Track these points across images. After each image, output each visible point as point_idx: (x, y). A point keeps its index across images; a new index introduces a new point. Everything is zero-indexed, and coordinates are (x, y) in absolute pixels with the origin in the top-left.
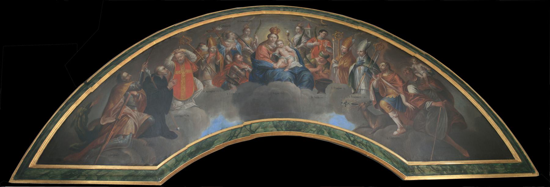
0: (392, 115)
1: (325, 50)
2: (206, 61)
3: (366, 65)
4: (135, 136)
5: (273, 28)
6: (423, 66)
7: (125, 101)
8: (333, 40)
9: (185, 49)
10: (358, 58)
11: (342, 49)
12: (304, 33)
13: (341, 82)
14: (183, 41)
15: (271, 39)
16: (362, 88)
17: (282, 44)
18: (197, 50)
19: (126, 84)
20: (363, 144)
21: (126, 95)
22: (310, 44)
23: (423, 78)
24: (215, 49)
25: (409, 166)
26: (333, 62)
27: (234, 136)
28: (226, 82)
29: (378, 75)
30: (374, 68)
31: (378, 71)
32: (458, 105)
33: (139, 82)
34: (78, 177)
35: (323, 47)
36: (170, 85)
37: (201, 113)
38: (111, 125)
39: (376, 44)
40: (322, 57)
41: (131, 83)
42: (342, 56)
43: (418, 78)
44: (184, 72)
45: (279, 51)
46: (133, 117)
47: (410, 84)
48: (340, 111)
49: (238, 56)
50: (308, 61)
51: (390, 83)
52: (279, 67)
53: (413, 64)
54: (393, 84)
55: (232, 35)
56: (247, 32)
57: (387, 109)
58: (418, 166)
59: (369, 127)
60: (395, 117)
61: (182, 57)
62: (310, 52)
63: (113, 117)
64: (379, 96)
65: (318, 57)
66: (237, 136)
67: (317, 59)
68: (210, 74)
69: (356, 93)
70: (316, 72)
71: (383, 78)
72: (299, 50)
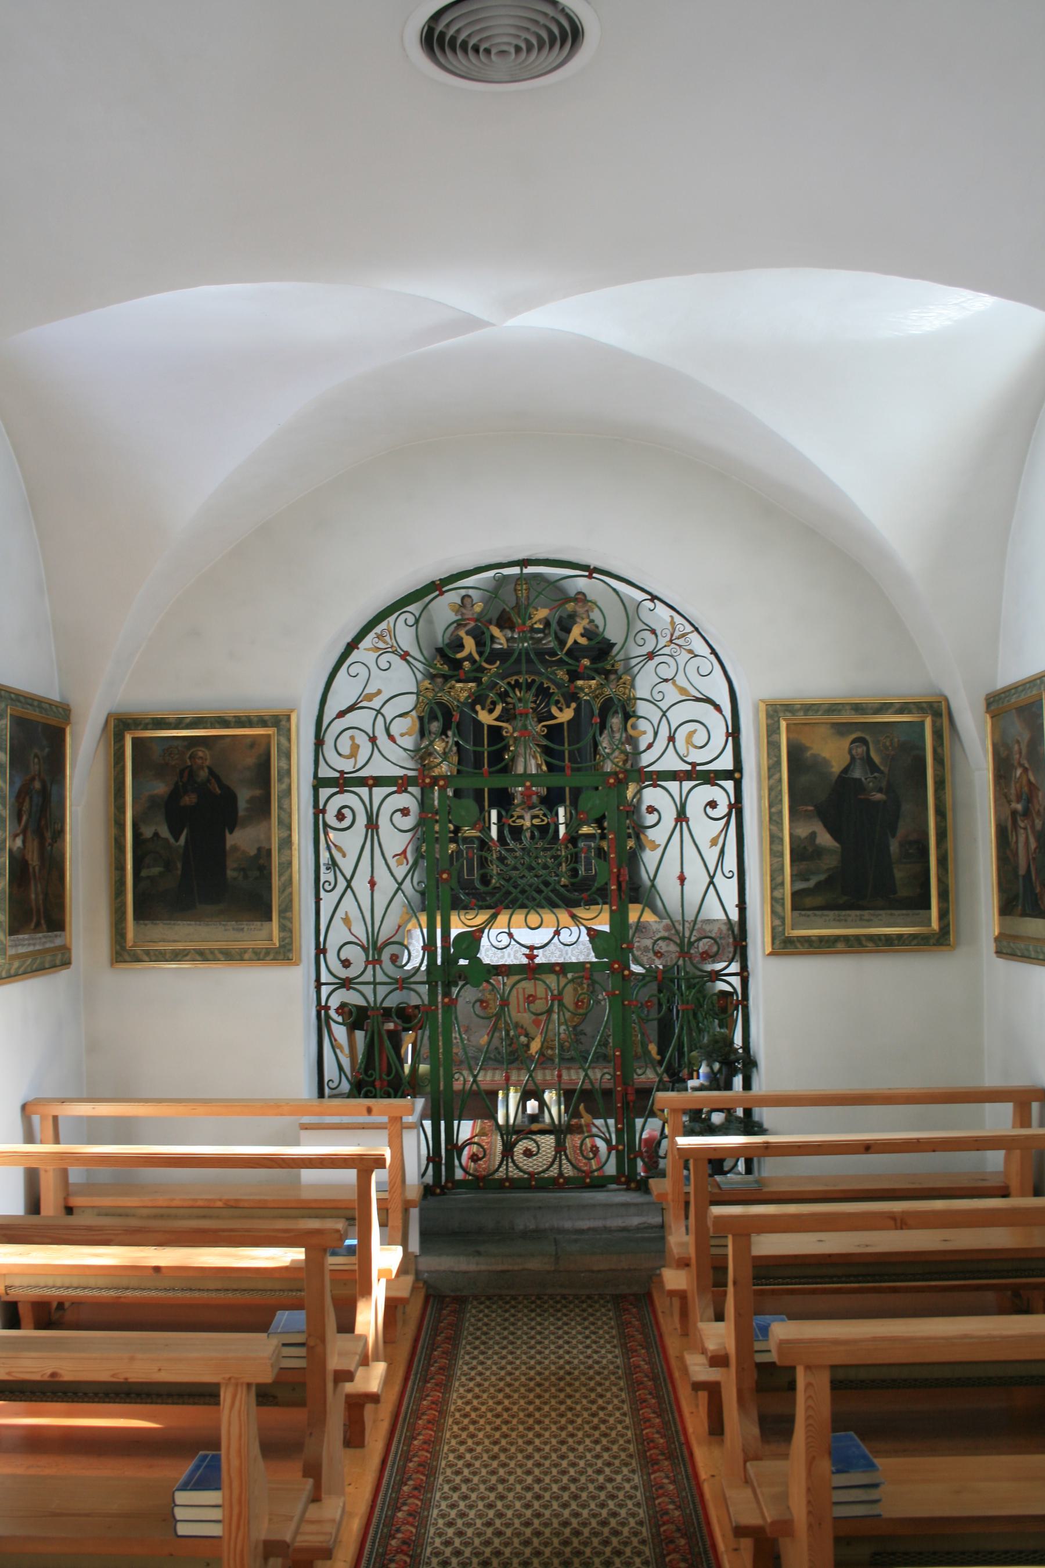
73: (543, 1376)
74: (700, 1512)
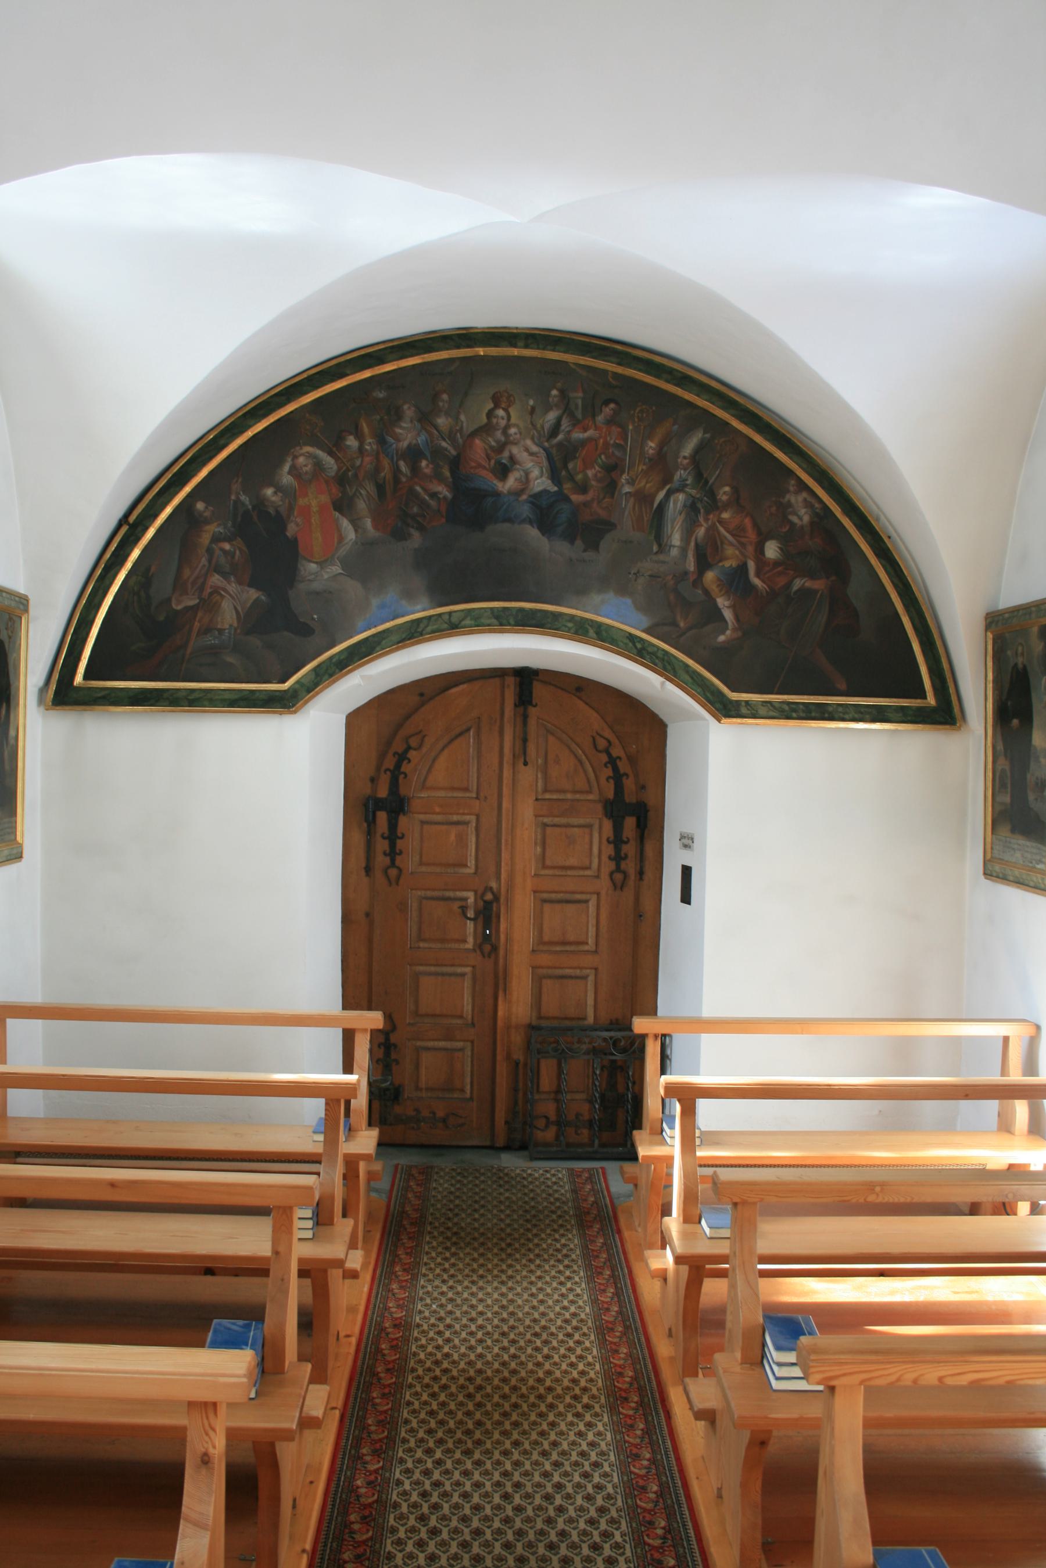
0: (722, 602)
1: (611, 451)
2: (356, 475)
3: (690, 491)
4: (239, 631)
5: (500, 392)
6: (809, 499)
7: (210, 561)
8: (631, 427)
9: (312, 446)
10: (678, 473)
11: (646, 449)
12: (568, 410)
13: (633, 527)
14: (308, 427)
15: (495, 421)
16: (673, 543)
17: (518, 436)
18: (335, 447)
19: (207, 528)
20: (657, 657)
21: (210, 551)
22: (578, 435)
23: (802, 527)
24: (375, 447)
25: (731, 701)
26: (623, 481)
27: (416, 632)
28: (399, 524)
29: (711, 516)
30: (705, 498)
31: (714, 505)
32: (856, 590)
33: (230, 522)
34: (157, 701)
35: (606, 444)
36: (291, 530)
37: (353, 588)
38: (194, 609)
39: (723, 440)
40: (602, 468)
41: (216, 524)
42: (644, 467)
43: (792, 524)
44: (315, 500)
45: (510, 452)
46: (230, 595)
47: (772, 538)
48: (623, 590)
49: (424, 463)
50: (571, 478)
51: (733, 535)
52: (508, 492)
53: (788, 491)
54: (737, 536)
55: (409, 411)
56: (441, 404)
57: (714, 588)
58: (747, 702)
59: (675, 624)
60: (726, 607)
61: (310, 466)
62: (577, 455)
63: (193, 595)
64: (703, 563)
65: (593, 467)
66: (423, 630)
67: (590, 473)
68: (366, 504)
69: (661, 553)
70: (586, 504)
71: (721, 522)
72: (554, 451)
73: (499, 1268)
74: (374, 1292)
